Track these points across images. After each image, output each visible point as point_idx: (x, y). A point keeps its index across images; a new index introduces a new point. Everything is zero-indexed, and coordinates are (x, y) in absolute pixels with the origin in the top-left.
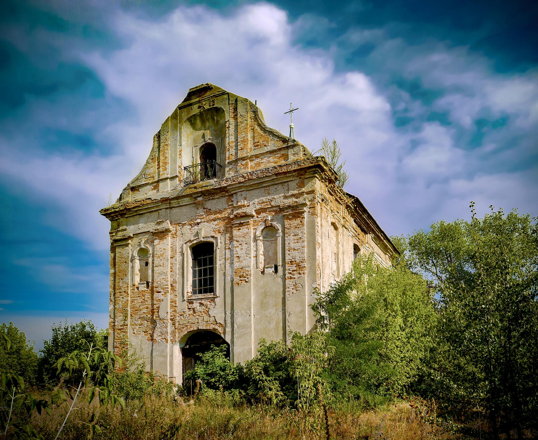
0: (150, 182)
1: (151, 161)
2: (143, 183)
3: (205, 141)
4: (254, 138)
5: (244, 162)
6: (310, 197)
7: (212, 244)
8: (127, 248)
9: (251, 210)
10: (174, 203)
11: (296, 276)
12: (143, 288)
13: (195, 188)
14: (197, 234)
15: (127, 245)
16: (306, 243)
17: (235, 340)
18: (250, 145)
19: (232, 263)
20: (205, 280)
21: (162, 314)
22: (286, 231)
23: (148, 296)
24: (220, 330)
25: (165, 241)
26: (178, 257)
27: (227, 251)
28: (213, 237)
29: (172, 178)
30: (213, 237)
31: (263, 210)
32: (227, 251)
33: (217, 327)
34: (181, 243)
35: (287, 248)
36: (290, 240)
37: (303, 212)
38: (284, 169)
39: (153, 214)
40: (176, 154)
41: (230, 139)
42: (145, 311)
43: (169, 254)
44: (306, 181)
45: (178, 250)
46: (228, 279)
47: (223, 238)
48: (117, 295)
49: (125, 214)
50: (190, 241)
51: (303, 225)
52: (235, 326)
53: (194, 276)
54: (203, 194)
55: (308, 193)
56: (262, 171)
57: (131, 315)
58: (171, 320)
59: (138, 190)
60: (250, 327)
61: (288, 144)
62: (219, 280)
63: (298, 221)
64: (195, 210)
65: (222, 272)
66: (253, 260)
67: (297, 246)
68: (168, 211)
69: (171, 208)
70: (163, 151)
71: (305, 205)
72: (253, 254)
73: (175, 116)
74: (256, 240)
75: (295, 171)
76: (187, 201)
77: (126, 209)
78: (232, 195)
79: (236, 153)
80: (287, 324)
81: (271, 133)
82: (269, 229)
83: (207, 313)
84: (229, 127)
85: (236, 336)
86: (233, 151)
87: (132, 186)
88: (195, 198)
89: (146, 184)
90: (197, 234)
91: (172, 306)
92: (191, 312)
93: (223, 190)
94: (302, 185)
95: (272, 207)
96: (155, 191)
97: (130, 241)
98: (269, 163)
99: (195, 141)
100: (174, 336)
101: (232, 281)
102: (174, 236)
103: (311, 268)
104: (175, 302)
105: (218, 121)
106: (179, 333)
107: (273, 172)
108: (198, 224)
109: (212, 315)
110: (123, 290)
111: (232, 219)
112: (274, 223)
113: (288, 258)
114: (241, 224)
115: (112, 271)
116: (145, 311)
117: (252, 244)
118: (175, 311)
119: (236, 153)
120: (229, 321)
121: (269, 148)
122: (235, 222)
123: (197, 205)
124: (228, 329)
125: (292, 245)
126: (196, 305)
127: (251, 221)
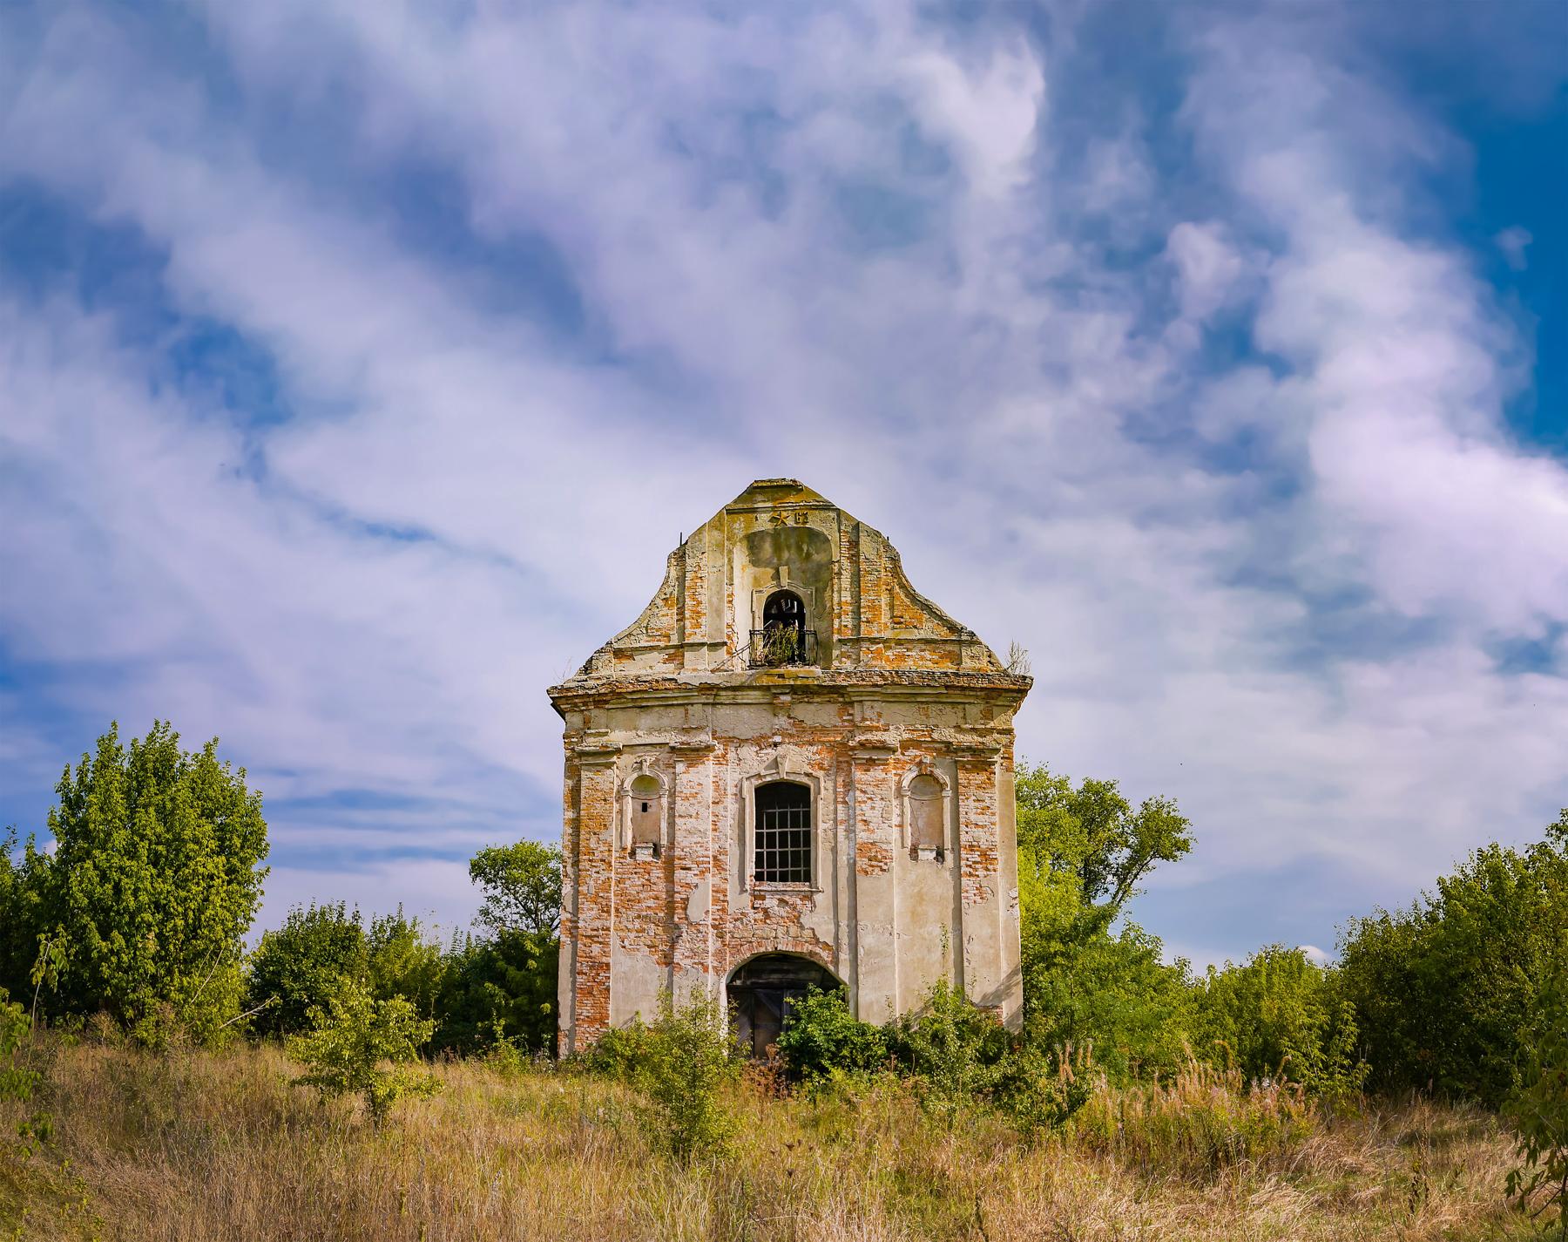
0: (662, 644)
1: (659, 602)
2: (643, 644)
3: (779, 585)
4: (892, 607)
5: (874, 647)
6: (1004, 739)
7: (805, 790)
8: (609, 772)
9: (892, 738)
10: (725, 696)
11: (981, 873)
12: (644, 855)
13: (781, 676)
14: (776, 764)
15: (609, 766)
16: (996, 819)
17: (861, 977)
18: (885, 618)
19: (850, 831)
20: (771, 855)
21: (694, 913)
22: (961, 790)
23: (658, 874)
24: (825, 956)
25: (701, 767)
26: (731, 806)
27: (840, 807)
28: (808, 775)
29: (714, 646)
30: (808, 775)
31: (916, 744)
32: (840, 807)
33: (818, 950)
34: (737, 776)
35: (962, 820)
36: (969, 807)
37: (993, 763)
38: (964, 682)
39: (673, 710)
40: (721, 600)
41: (842, 593)
42: (651, 903)
43: (709, 794)
44: (995, 709)
45: (731, 790)
46: (843, 860)
47: (830, 785)
48: (584, 865)
49: (607, 702)
50: (759, 776)
51: (993, 785)
52: (861, 951)
53: (759, 844)
54: (794, 690)
55: (1000, 732)
56: (921, 675)
57: (617, 910)
58: (714, 927)
59: (631, 657)
60: (892, 956)
61: (959, 638)
62: (824, 860)
63: (983, 777)
64: (770, 716)
65: (829, 846)
66: (895, 832)
67: (981, 820)
68: (709, 709)
69: (714, 704)
70: (694, 587)
71: (997, 751)
72: (895, 820)
73: (717, 523)
74: (899, 794)
75: (982, 689)
76: (754, 696)
77: (613, 692)
78: (851, 703)
79: (857, 627)
80: (965, 956)
81: (927, 607)
82: (926, 781)
83: (797, 920)
84: (840, 574)
85: (861, 970)
86: (848, 620)
87: (616, 646)
88: (775, 696)
89: (652, 648)
90: (776, 764)
91: (716, 901)
92: (760, 916)
93: (837, 690)
94: (988, 715)
95: (934, 741)
96: (671, 666)
97: (615, 759)
98: (920, 662)
99: (756, 580)
100: (721, 960)
101: (852, 866)
102: (722, 760)
103: (1006, 861)
104: (724, 892)
105: (809, 555)
106: (732, 955)
107: (942, 681)
108: (776, 745)
109: (807, 922)
110: (598, 855)
111: (853, 749)
112: (938, 772)
113: (964, 838)
114: (871, 762)
115: (570, 815)
116: (651, 903)
117: (895, 802)
118: (723, 910)
119: (857, 627)
120: (844, 940)
121: (923, 634)
122: (853, 756)
123: (774, 708)
124: (844, 956)
125: (973, 817)
126: (771, 902)
127: (891, 758)
